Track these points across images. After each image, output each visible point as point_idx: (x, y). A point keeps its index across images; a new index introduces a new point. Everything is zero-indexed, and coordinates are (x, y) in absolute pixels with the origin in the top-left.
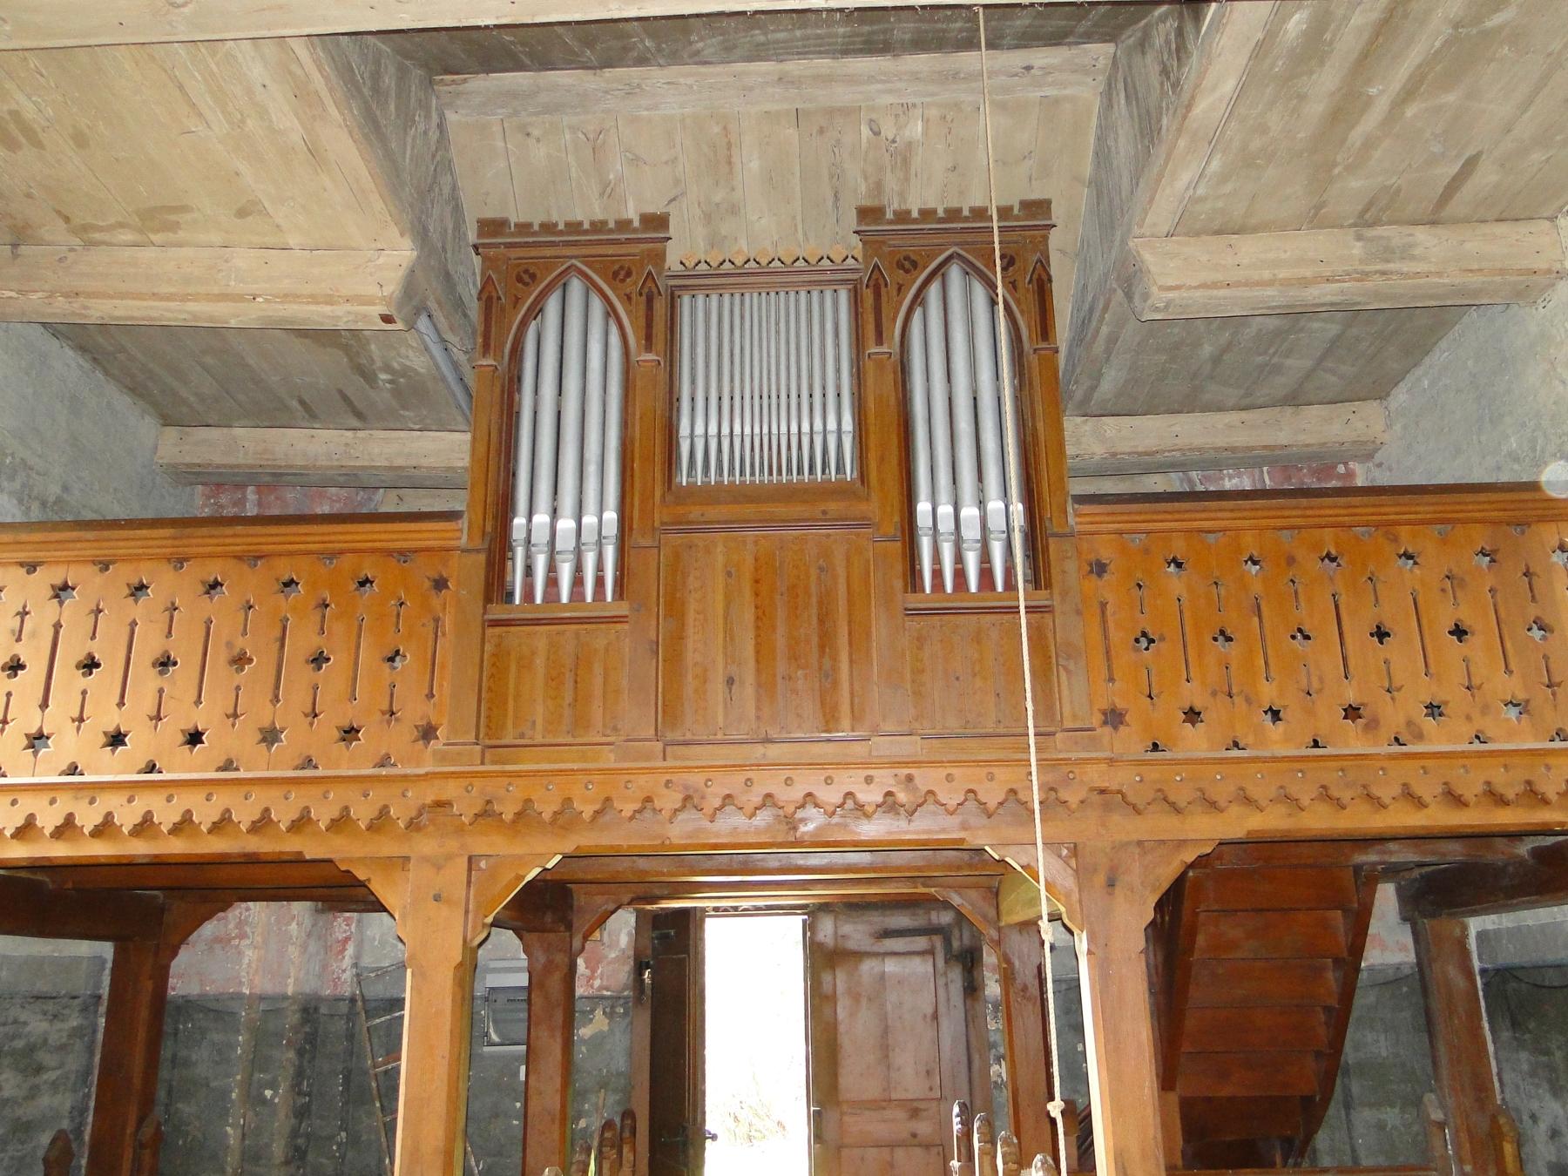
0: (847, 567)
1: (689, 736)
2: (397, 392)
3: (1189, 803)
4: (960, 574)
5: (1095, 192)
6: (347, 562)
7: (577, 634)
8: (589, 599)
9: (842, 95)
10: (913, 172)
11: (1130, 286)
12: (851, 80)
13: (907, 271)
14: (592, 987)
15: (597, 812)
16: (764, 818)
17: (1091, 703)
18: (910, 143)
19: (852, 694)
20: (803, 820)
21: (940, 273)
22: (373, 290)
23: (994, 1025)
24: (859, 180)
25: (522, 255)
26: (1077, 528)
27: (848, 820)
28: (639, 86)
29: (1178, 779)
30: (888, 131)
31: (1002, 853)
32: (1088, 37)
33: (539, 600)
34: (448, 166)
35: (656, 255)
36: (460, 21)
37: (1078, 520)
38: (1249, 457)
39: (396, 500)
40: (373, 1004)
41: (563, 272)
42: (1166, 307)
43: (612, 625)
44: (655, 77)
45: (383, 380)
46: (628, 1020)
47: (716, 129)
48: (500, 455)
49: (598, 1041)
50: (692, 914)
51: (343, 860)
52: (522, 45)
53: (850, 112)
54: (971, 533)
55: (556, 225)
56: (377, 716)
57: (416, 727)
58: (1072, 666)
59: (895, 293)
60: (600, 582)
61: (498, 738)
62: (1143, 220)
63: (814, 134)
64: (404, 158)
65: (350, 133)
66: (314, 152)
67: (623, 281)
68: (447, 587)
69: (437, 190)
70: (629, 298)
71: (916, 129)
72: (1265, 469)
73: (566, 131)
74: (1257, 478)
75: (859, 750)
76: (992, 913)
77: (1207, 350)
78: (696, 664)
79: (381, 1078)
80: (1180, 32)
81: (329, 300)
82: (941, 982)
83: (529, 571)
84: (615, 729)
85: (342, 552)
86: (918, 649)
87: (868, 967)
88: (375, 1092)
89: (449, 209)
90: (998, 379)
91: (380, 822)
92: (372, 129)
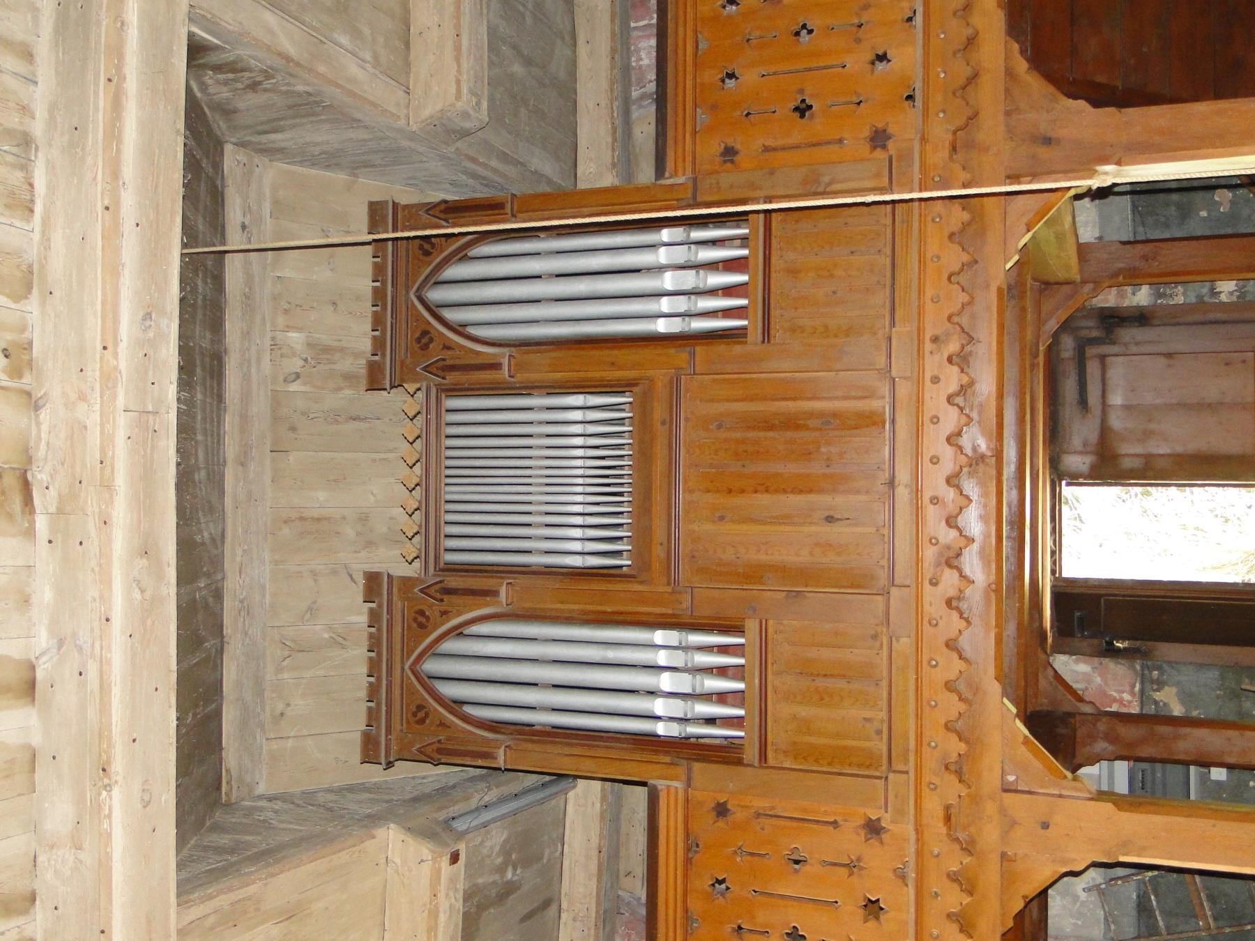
0: (718, 401)
1: (884, 563)
2: (526, 862)
3: (968, 64)
4: (728, 291)
5: (363, 170)
6: (695, 905)
7: (778, 673)
8: (741, 661)
9: (260, 406)
10: (335, 344)
11: (454, 132)
12: (246, 397)
13: (431, 340)
14: (1130, 702)
15: (961, 657)
16: (971, 487)
17: (862, 160)
18: (309, 345)
19: (847, 398)
20: (975, 449)
21: (435, 309)
22: (426, 868)
23: (1180, 296)
24: (341, 396)
25: (398, 718)
26: (689, 174)
27: (976, 403)
28: (242, 602)
29: (942, 75)
30: (296, 365)
31: (1013, 251)
32: (218, 165)
33: (741, 712)
34: (309, 797)
35: (404, 585)
36: (171, 744)
37: (680, 173)
38: (622, 36)
39: (630, 878)
40: (1143, 929)
41: (417, 678)
42: (476, 95)
43: (770, 637)
44: (233, 585)
45: (513, 876)
46: (1165, 667)
47: (286, 531)
48: (593, 746)
49: (1186, 697)
50: (1058, 590)
51: (1003, 924)
52: (197, 706)
53: (277, 400)
54: (689, 280)
55: (371, 684)
56: (854, 879)
57: (867, 840)
58: (826, 179)
59: (450, 353)
60: (723, 649)
61: (881, 757)
62: (393, 115)
63: (296, 436)
64: (301, 831)
65: (273, 875)
66: (289, 914)
67: (428, 618)
68: (725, 803)
69: (331, 805)
70: (444, 613)
71: (296, 338)
72: (633, 25)
73: (280, 677)
74: (641, 34)
75: (903, 390)
76: (1066, 289)
77: (517, 69)
78: (811, 553)
79: (1221, 923)
80: (218, 68)
81: (434, 914)
82: (1134, 349)
83: (711, 721)
84: (875, 637)
85: (686, 911)
86: (803, 332)
87: (1117, 422)
88: (1234, 930)
89: (349, 796)
90: (539, 254)
91: (965, 882)
92: (268, 856)
